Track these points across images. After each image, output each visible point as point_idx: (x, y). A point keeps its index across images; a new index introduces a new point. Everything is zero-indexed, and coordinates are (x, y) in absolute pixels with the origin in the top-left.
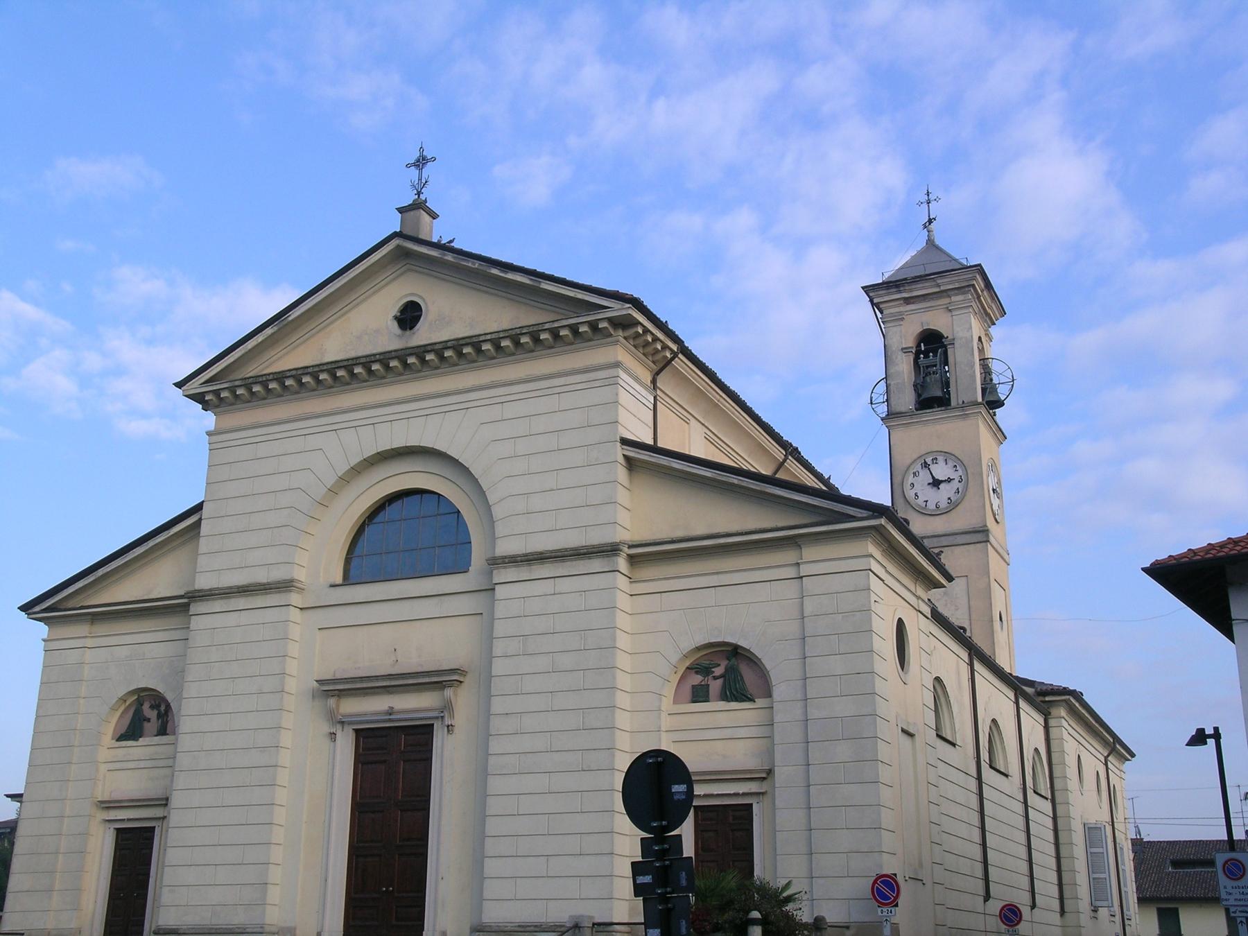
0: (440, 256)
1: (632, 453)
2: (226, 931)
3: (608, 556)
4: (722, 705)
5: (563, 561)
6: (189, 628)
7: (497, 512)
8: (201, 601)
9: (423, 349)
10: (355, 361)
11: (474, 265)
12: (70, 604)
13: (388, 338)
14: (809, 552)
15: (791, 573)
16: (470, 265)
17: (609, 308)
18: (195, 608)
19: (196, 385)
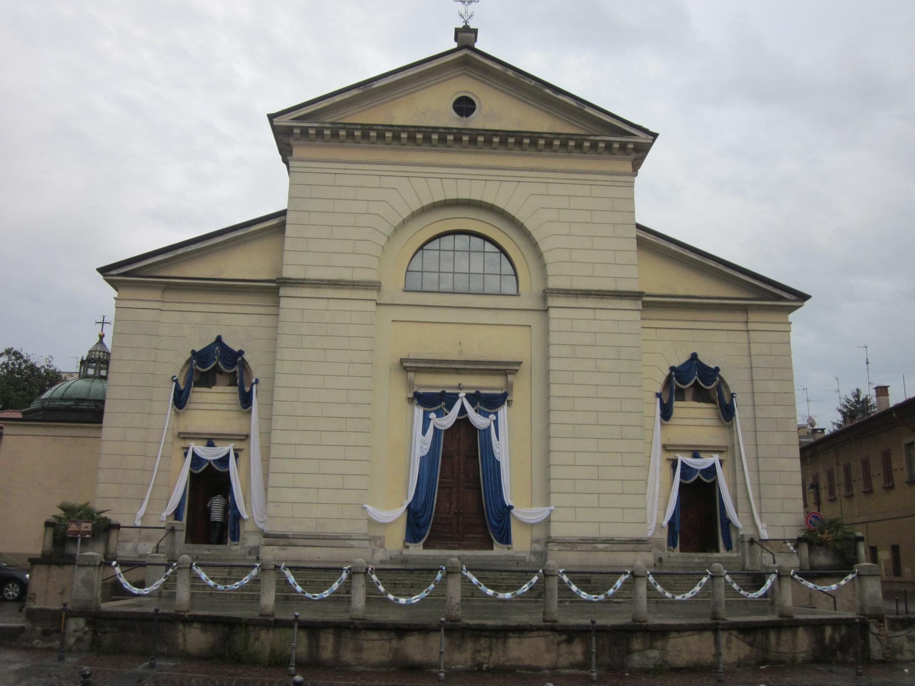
0: (502, 70)
1: (642, 234)
2: (331, 537)
3: (635, 299)
4: (695, 404)
5: (602, 298)
6: (279, 306)
7: (548, 257)
8: (290, 286)
9: (493, 133)
10: (419, 129)
11: (531, 82)
12: (141, 273)
13: (451, 120)
14: (753, 316)
15: (742, 327)
16: (528, 82)
17: (637, 136)
18: (283, 291)
19: (286, 119)
